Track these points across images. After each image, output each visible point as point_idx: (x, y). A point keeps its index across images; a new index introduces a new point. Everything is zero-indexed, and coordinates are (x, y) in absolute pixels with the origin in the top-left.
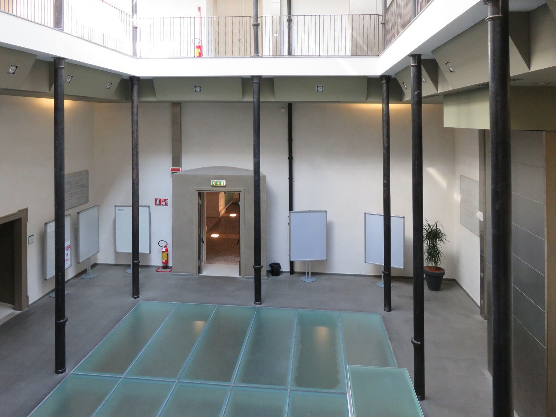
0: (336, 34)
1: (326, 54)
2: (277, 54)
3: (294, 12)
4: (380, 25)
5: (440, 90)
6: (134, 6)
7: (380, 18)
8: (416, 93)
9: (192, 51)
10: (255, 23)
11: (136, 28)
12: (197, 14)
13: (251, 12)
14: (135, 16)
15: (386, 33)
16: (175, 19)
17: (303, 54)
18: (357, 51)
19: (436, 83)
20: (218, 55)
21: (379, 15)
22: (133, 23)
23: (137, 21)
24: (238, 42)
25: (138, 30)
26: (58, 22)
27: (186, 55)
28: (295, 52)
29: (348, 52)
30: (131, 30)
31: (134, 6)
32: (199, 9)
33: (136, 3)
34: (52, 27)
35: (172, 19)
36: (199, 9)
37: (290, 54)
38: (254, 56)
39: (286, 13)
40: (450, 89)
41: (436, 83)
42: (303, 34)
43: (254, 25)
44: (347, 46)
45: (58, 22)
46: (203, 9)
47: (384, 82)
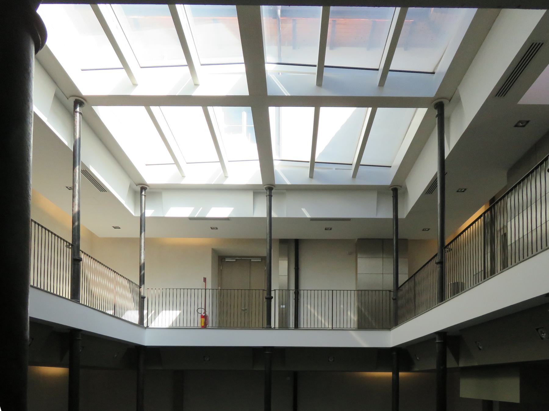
0: (342, 306)
1: (338, 326)
2: (284, 326)
3: (303, 285)
4: (392, 300)
5: (461, 365)
6: (142, 277)
7: (392, 293)
8: (442, 368)
9: (199, 322)
10: (268, 296)
11: (144, 298)
12: (201, 285)
13: (264, 286)
14: (142, 287)
15: (397, 308)
16: (182, 290)
17: (309, 326)
18: (364, 324)
19: (457, 360)
20: (222, 325)
21: (390, 291)
22: (140, 293)
23: (144, 291)
24: (243, 313)
25: (146, 300)
26: (75, 295)
27: (185, 325)
28: (303, 323)
29: (354, 324)
30: (137, 299)
31: (142, 277)
32: (205, 280)
33: (144, 274)
34: (70, 298)
35: (179, 290)
36: (205, 280)
37: (297, 326)
38: (267, 327)
39: (293, 287)
40: (476, 364)
41: (457, 360)
42: (309, 307)
43: (266, 298)
44: (353, 317)
45: (75, 295)
46: (209, 280)
47: (394, 353)
